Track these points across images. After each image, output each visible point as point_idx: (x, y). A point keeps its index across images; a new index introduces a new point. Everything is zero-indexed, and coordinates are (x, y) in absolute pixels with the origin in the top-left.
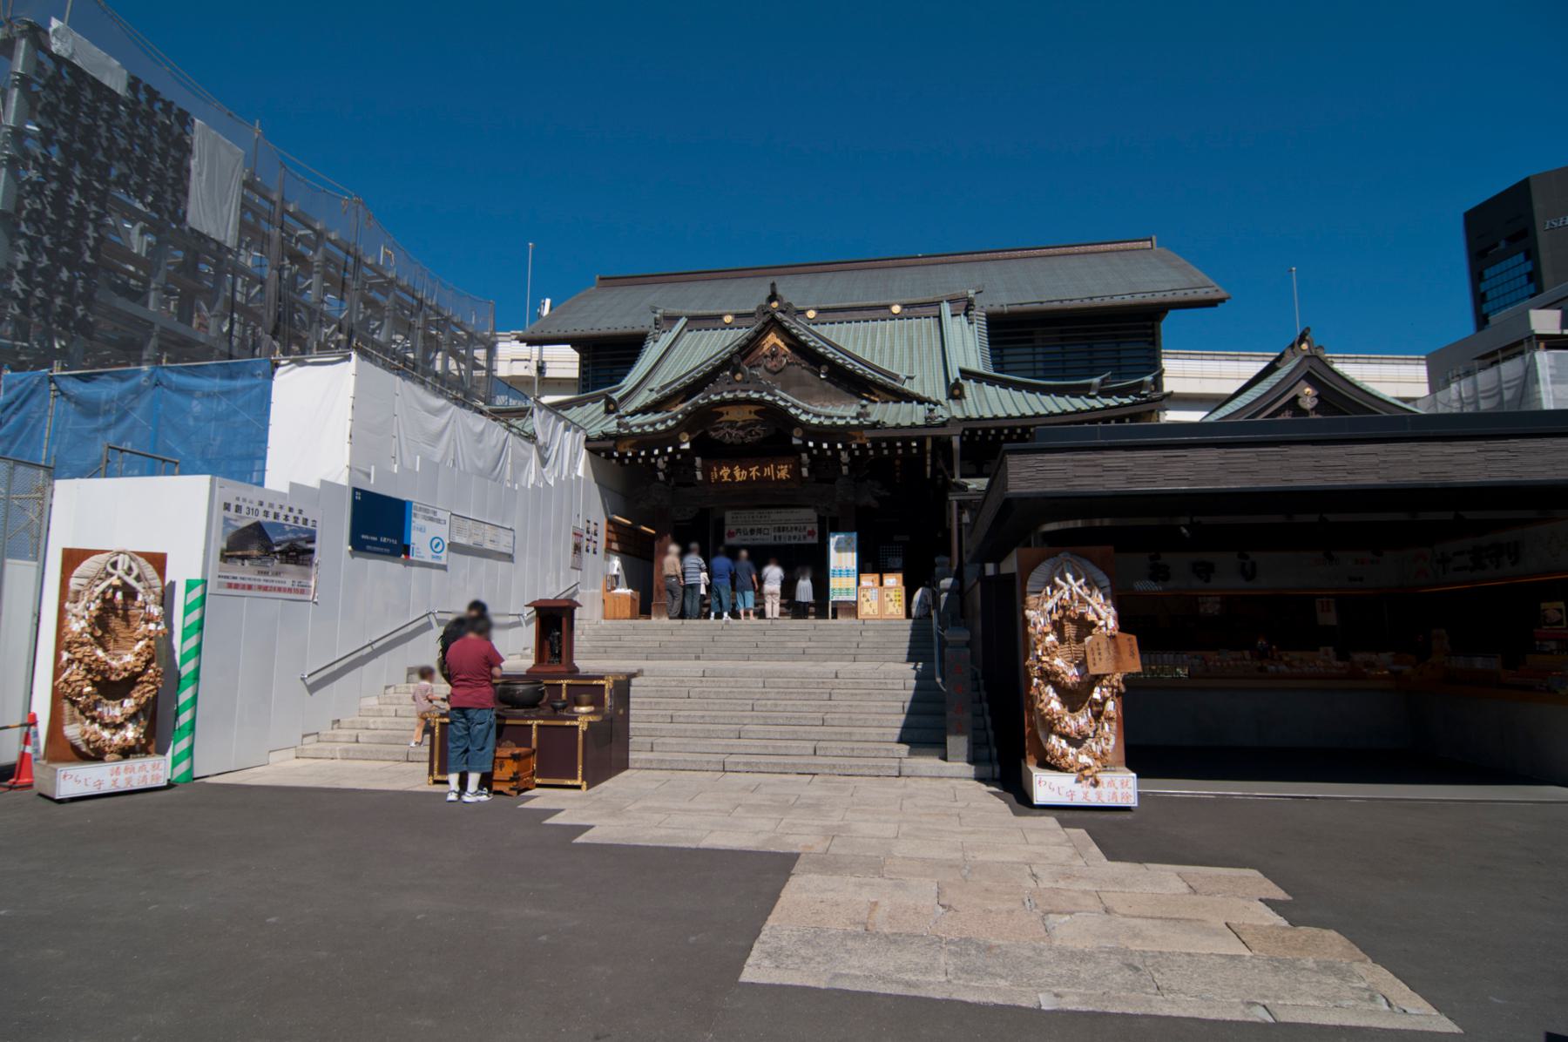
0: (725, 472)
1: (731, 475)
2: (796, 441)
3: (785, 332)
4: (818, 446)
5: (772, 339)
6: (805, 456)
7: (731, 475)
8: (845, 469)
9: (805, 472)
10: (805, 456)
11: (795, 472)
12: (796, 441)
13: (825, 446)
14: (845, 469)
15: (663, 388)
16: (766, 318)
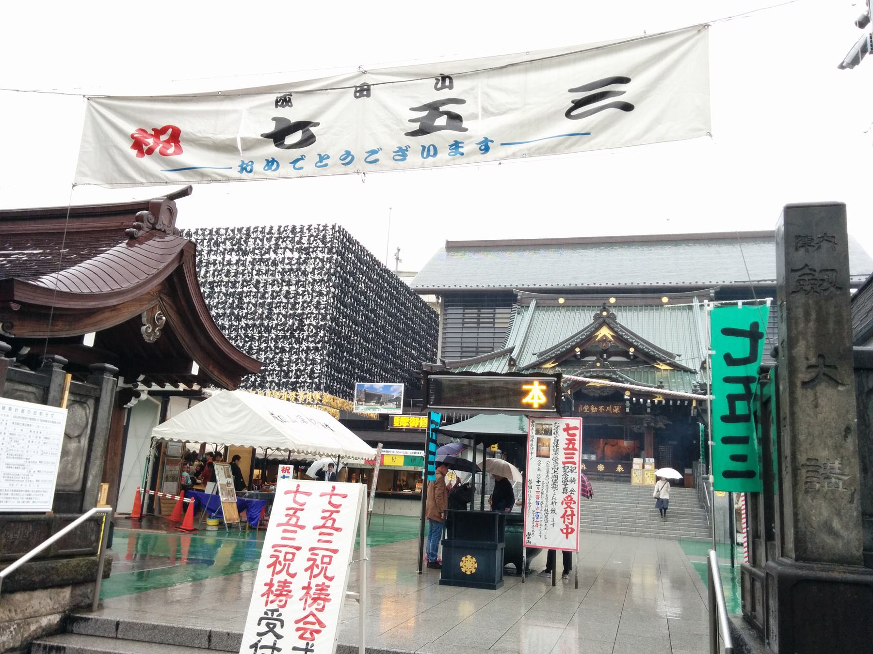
0: (586, 408)
1: (589, 410)
2: (626, 397)
3: (611, 329)
4: (638, 400)
5: (605, 332)
6: (628, 402)
7: (589, 410)
8: (649, 410)
9: (628, 410)
10: (628, 402)
11: (623, 409)
12: (626, 397)
13: (641, 400)
14: (649, 410)
15: (541, 354)
16: (601, 320)
